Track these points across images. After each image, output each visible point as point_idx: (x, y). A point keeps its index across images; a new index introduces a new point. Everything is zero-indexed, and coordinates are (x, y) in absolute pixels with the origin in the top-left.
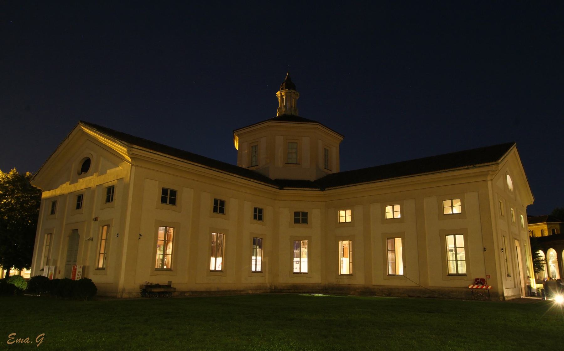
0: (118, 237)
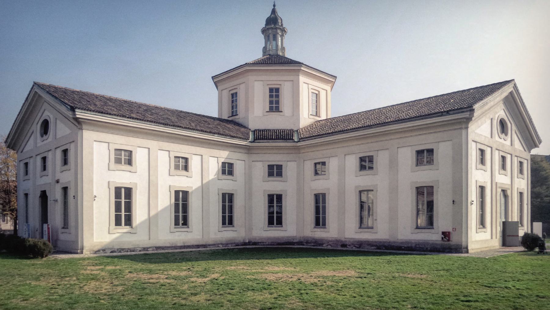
0: (453, 203)
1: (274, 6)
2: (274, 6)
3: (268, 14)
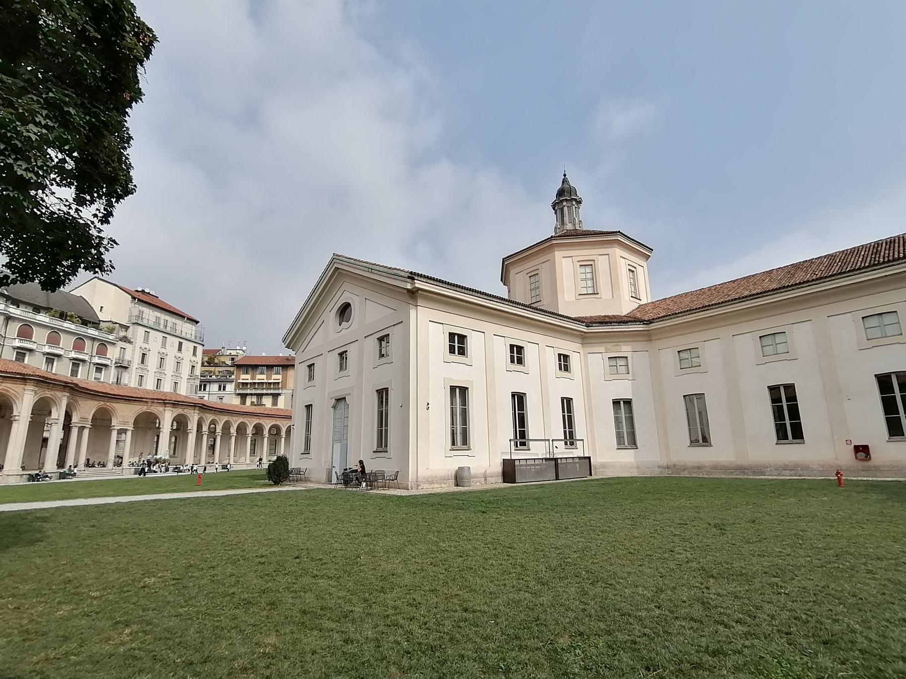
1: (565, 175)
2: (565, 175)
3: (559, 186)
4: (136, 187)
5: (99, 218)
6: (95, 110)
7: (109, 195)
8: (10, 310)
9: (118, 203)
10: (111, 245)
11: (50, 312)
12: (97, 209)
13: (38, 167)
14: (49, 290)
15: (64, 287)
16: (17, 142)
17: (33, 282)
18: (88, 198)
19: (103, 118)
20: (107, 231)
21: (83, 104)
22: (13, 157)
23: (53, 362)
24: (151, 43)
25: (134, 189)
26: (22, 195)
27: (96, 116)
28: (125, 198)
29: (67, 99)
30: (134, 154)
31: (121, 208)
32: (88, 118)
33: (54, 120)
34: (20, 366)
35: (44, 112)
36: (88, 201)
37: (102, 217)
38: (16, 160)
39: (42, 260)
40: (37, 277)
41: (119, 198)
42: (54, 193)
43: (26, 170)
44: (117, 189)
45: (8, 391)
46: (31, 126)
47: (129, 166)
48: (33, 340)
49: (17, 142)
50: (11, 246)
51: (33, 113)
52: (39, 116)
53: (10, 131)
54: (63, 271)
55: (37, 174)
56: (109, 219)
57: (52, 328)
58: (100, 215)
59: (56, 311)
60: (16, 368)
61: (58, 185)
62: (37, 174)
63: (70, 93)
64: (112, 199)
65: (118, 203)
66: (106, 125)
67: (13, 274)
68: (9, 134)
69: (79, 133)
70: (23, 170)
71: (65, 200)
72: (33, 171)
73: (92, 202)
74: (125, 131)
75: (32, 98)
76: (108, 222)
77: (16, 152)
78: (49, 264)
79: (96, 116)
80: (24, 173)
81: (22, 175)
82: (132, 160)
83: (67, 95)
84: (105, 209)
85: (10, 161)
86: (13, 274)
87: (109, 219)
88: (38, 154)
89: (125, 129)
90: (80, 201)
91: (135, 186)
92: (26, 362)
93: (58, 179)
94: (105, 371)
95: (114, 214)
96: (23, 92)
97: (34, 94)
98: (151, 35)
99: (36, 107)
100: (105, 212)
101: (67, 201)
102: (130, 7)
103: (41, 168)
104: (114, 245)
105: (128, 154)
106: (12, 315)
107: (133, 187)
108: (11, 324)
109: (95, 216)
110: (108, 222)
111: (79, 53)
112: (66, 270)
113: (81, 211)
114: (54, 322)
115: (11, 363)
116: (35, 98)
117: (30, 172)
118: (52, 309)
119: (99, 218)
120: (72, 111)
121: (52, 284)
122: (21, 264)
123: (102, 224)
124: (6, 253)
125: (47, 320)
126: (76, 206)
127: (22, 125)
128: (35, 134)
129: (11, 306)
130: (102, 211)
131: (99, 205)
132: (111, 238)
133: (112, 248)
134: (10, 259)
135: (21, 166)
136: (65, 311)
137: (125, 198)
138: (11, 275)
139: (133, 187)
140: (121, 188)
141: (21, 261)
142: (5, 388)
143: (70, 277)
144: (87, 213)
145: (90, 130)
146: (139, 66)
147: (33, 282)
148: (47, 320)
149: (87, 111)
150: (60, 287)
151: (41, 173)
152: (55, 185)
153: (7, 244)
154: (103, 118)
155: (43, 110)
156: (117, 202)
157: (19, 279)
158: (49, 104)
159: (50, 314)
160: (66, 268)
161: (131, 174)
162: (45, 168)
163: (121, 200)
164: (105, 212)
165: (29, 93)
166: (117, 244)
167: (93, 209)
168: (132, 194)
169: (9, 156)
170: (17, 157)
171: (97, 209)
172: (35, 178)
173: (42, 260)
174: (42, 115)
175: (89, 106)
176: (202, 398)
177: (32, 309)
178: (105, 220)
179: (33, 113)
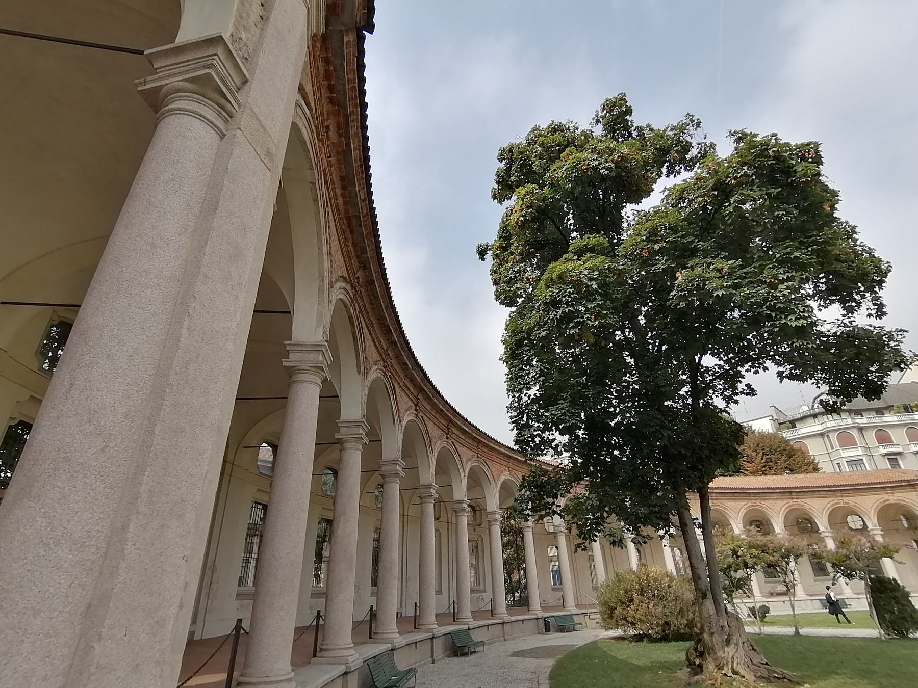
4: (889, 263)
5: (874, 315)
6: (811, 239)
7: (870, 289)
8: (858, 421)
9: (882, 289)
10: (901, 335)
11: (893, 409)
12: (868, 309)
13: (802, 312)
14: (874, 399)
15: (886, 391)
16: (780, 305)
17: (857, 397)
18: (854, 304)
19: (820, 240)
20: (888, 324)
21: (801, 243)
22: (783, 317)
23: (898, 462)
24: (817, 151)
25: (890, 266)
26: (805, 340)
27: (815, 243)
28: (886, 280)
29: (789, 249)
30: (865, 238)
31: (886, 294)
32: (810, 249)
33: (790, 271)
34: (900, 472)
35: (781, 271)
36: (855, 306)
37: (877, 313)
38: (786, 317)
39: (852, 375)
40: (858, 391)
41: (880, 283)
42: (825, 321)
43: (796, 319)
44: (873, 278)
45: (904, 501)
46: (780, 287)
47: (870, 251)
48: (895, 442)
49: (780, 305)
50: (823, 376)
51: (775, 277)
52: (780, 275)
53: (771, 301)
54: (876, 377)
55: (805, 318)
56: (883, 310)
57: (906, 425)
58: (873, 312)
59: (898, 407)
60: (896, 476)
61: (825, 307)
62: (805, 318)
63: (789, 244)
64: (875, 290)
65: (882, 289)
66: (826, 242)
67: (838, 397)
68: (772, 303)
69: (811, 265)
70: (795, 321)
71: (836, 321)
72: (801, 318)
73: (859, 305)
74: (845, 226)
75: (770, 268)
76: (885, 314)
77: (783, 313)
78: (860, 376)
79: (815, 243)
80: (796, 323)
81: (796, 325)
82: (869, 244)
83: (786, 248)
84: (874, 305)
85: (783, 321)
86: (838, 397)
87: (883, 310)
88: (796, 303)
89: (845, 224)
90: (850, 310)
91: (888, 263)
92: (903, 467)
93: (822, 303)
94: (902, 460)
95: (884, 303)
96: (762, 269)
97: (768, 264)
98: (813, 146)
99: (775, 271)
100: (876, 307)
101: (838, 320)
102: (784, 149)
103: (804, 311)
104: (904, 333)
105: (862, 242)
106: (862, 425)
107: (886, 265)
108: (866, 434)
109: (870, 315)
110: (885, 314)
111: (776, 213)
112: (877, 374)
113: (854, 321)
114: (904, 418)
115: (889, 471)
116: (771, 266)
117: (799, 319)
118: (893, 406)
119: (874, 315)
120: (797, 254)
121: (874, 391)
122: (838, 386)
123: (880, 319)
124: (824, 383)
125: (895, 419)
126: (847, 320)
127: (775, 290)
128: (785, 289)
129: (856, 418)
130: (873, 307)
131: (867, 305)
132: (896, 329)
133: (904, 337)
134: (829, 387)
135: (791, 319)
136: (907, 403)
137: (886, 280)
138: (837, 400)
139: (886, 265)
140: (876, 275)
141: (837, 384)
142: (899, 498)
143: (885, 379)
144: (862, 319)
145: (818, 256)
146: (820, 178)
147: (857, 397)
148: (895, 419)
149: (807, 245)
150: (882, 393)
151: (806, 315)
152: (823, 309)
153: (819, 375)
154: (820, 240)
155: (780, 270)
156: (881, 289)
157: (845, 399)
158: (782, 262)
159: (894, 411)
160: (876, 372)
161: (876, 256)
162: (806, 309)
163: (883, 285)
164: (876, 307)
165: (766, 265)
166: (906, 331)
167: (863, 311)
168: (890, 271)
169: (781, 318)
170: (785, 315)
171: (868, 309)
172: (805, 322)
173: (852, 375)
174: (781, 274)
175: (806, 240)
176: (855, 463)
177: (874, 413)
178: (880, 312)
179: (775, 277)
